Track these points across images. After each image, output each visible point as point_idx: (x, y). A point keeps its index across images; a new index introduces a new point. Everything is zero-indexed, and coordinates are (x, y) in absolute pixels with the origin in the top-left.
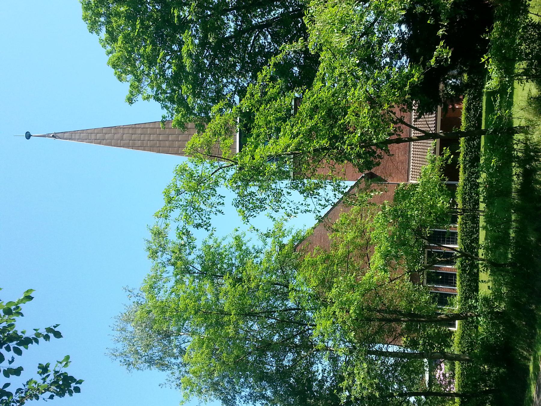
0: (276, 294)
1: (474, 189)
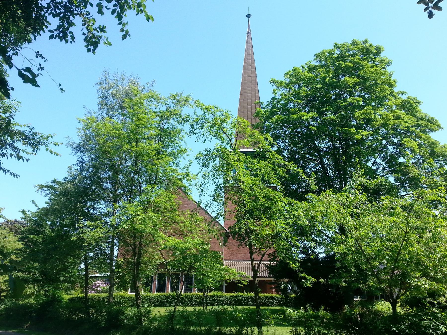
0: (150, 177)
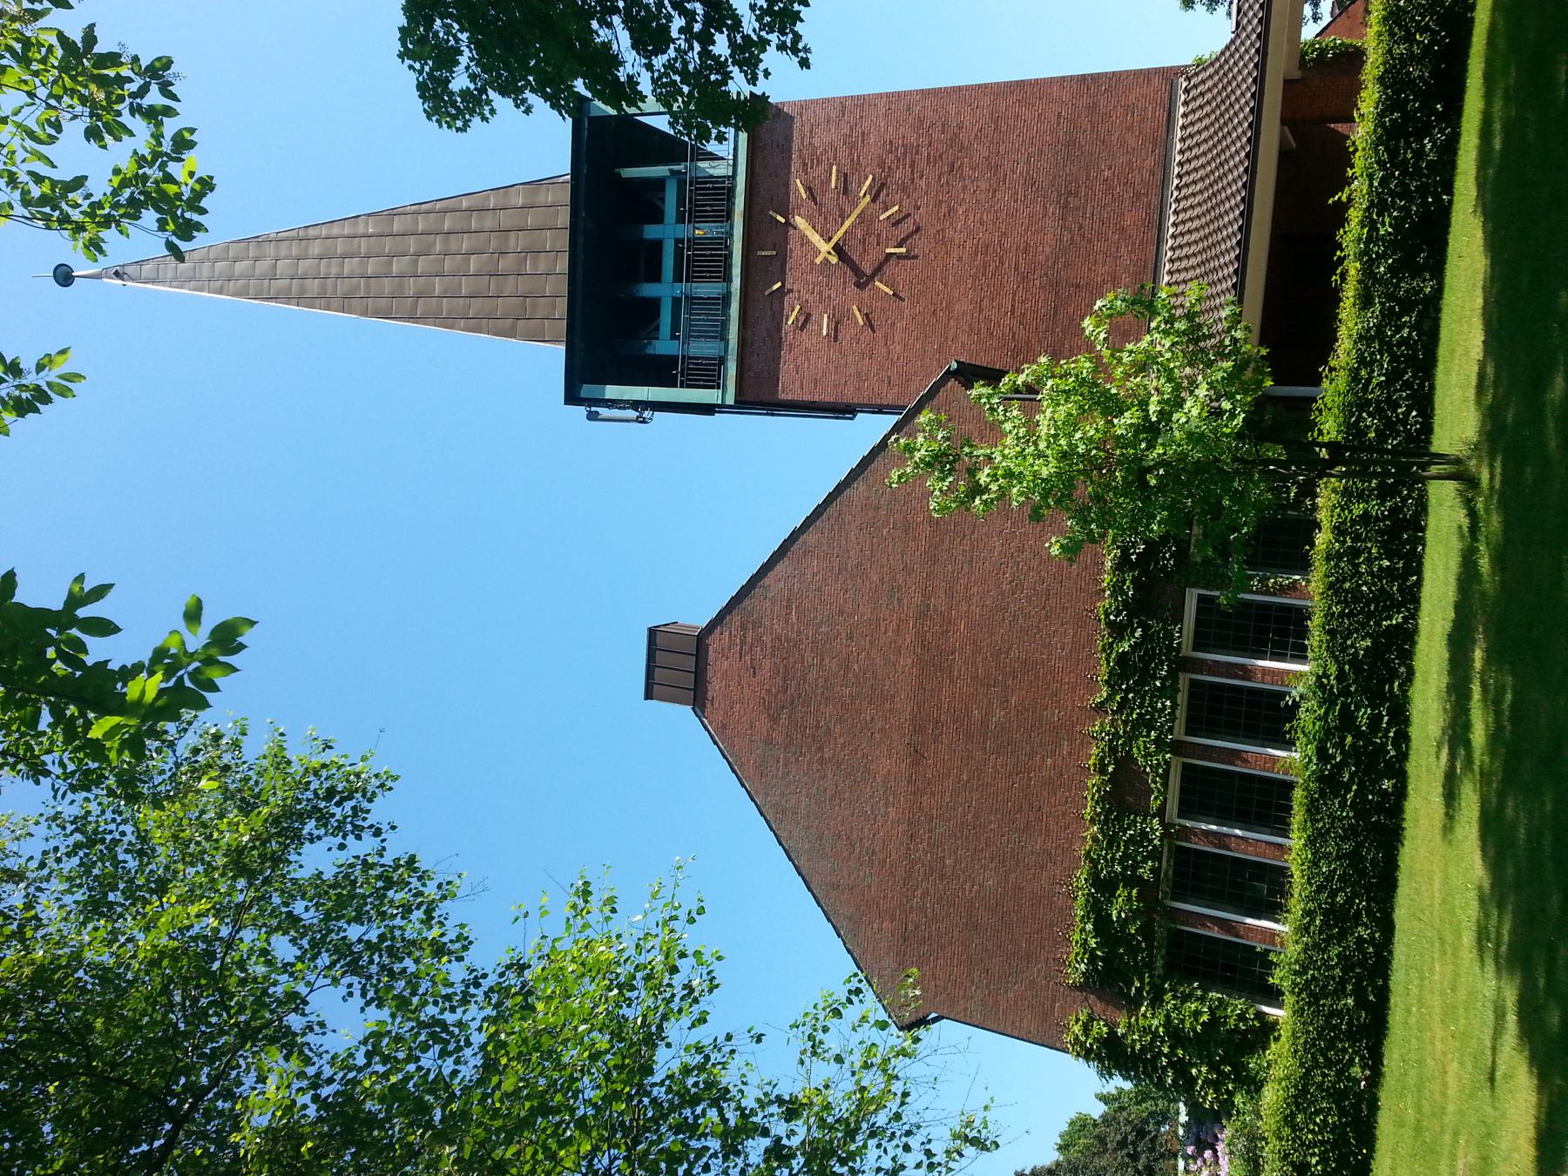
1: (1407, 385)
